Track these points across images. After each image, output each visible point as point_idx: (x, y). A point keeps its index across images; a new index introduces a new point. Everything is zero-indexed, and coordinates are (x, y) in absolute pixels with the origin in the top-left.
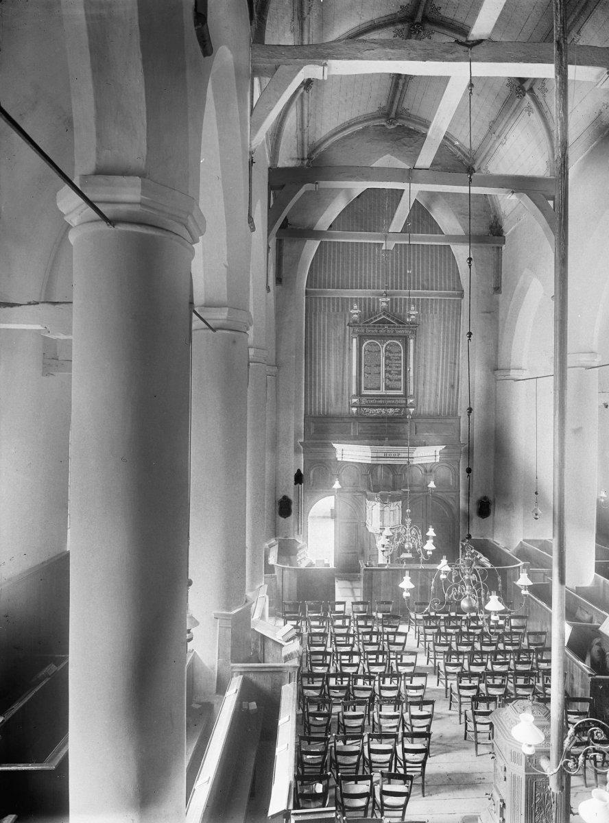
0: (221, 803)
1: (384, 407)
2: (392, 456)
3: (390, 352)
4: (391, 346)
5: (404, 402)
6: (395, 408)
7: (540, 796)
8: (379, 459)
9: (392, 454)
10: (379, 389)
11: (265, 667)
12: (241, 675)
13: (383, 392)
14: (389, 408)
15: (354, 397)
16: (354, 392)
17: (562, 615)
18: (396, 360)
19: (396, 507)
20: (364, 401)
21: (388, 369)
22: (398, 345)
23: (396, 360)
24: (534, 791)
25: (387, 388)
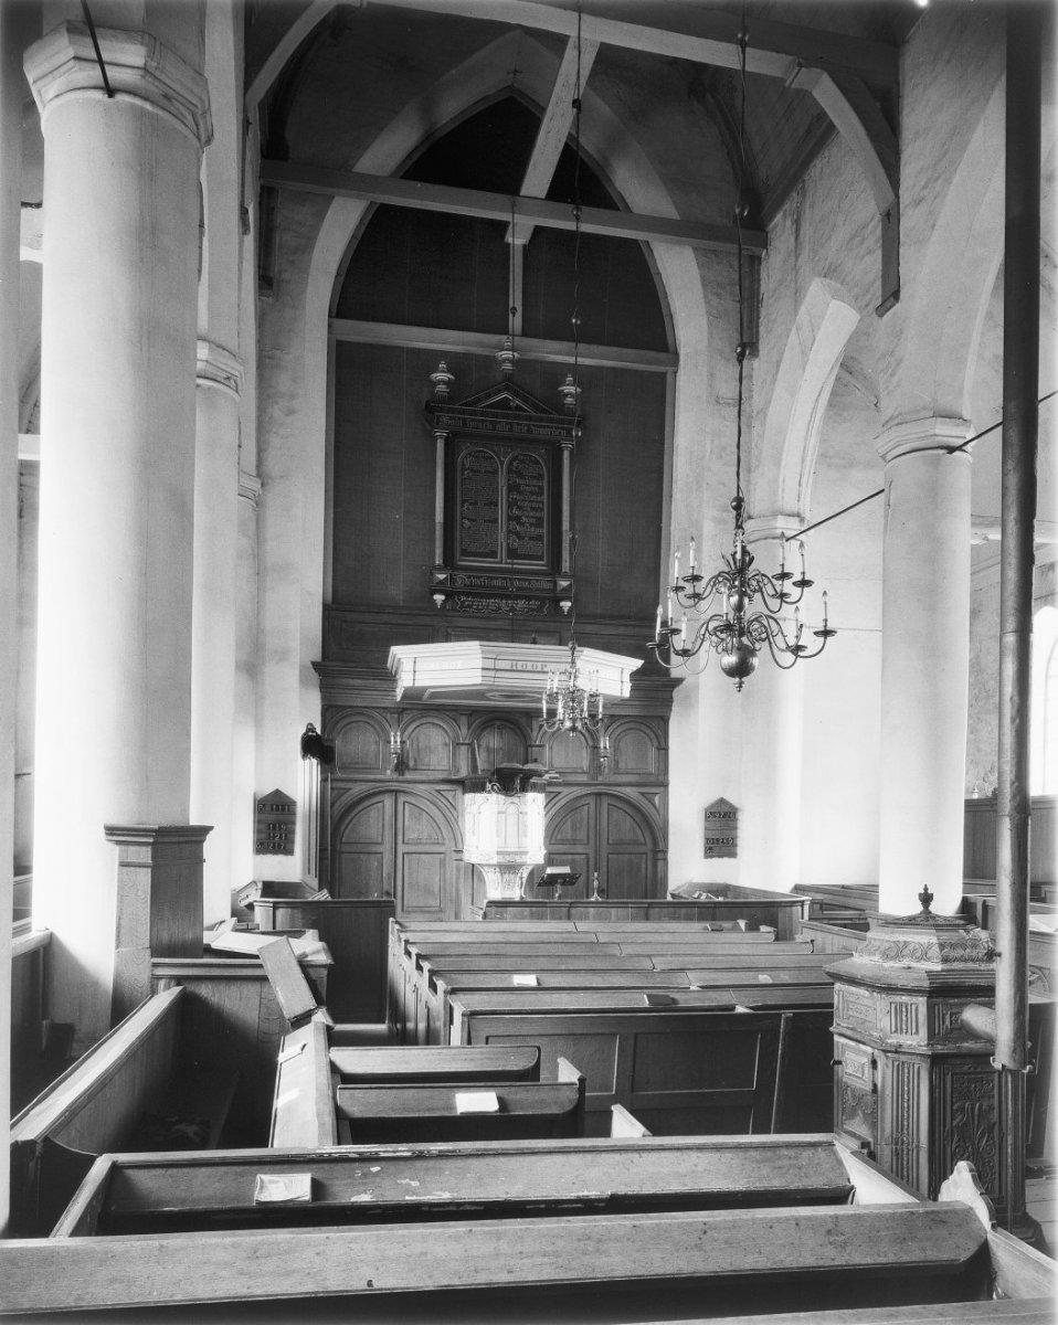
0: (286, 19)
1: (507, 597)
2: (529, 668)
3: (520, 475)
4: (523, 462)
5: (549, 586)
6: (528, 598)
7: (962, 1109)
8: (499, 674)
9: (539, 665)
10: (493, 554)
11: (119, 835)
12: (178, 985)
13: (502, 562)
14: (517, 597)
15: (441, 569)
16: (438, 561)
17: (999, 910)
18: (532, 493)
19: (205, 942)
20: (461, 578)
21: (515, 512)
22: (537, 463)
23: (532, 493)
24: (949, 1098)
25: (512, 554)
